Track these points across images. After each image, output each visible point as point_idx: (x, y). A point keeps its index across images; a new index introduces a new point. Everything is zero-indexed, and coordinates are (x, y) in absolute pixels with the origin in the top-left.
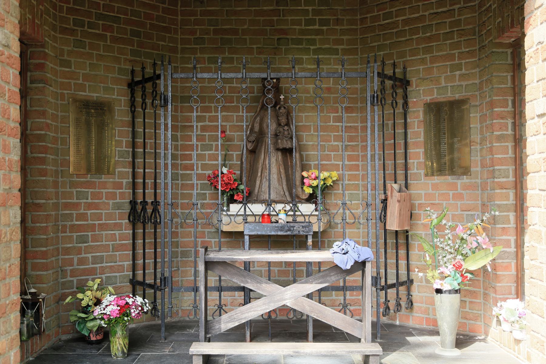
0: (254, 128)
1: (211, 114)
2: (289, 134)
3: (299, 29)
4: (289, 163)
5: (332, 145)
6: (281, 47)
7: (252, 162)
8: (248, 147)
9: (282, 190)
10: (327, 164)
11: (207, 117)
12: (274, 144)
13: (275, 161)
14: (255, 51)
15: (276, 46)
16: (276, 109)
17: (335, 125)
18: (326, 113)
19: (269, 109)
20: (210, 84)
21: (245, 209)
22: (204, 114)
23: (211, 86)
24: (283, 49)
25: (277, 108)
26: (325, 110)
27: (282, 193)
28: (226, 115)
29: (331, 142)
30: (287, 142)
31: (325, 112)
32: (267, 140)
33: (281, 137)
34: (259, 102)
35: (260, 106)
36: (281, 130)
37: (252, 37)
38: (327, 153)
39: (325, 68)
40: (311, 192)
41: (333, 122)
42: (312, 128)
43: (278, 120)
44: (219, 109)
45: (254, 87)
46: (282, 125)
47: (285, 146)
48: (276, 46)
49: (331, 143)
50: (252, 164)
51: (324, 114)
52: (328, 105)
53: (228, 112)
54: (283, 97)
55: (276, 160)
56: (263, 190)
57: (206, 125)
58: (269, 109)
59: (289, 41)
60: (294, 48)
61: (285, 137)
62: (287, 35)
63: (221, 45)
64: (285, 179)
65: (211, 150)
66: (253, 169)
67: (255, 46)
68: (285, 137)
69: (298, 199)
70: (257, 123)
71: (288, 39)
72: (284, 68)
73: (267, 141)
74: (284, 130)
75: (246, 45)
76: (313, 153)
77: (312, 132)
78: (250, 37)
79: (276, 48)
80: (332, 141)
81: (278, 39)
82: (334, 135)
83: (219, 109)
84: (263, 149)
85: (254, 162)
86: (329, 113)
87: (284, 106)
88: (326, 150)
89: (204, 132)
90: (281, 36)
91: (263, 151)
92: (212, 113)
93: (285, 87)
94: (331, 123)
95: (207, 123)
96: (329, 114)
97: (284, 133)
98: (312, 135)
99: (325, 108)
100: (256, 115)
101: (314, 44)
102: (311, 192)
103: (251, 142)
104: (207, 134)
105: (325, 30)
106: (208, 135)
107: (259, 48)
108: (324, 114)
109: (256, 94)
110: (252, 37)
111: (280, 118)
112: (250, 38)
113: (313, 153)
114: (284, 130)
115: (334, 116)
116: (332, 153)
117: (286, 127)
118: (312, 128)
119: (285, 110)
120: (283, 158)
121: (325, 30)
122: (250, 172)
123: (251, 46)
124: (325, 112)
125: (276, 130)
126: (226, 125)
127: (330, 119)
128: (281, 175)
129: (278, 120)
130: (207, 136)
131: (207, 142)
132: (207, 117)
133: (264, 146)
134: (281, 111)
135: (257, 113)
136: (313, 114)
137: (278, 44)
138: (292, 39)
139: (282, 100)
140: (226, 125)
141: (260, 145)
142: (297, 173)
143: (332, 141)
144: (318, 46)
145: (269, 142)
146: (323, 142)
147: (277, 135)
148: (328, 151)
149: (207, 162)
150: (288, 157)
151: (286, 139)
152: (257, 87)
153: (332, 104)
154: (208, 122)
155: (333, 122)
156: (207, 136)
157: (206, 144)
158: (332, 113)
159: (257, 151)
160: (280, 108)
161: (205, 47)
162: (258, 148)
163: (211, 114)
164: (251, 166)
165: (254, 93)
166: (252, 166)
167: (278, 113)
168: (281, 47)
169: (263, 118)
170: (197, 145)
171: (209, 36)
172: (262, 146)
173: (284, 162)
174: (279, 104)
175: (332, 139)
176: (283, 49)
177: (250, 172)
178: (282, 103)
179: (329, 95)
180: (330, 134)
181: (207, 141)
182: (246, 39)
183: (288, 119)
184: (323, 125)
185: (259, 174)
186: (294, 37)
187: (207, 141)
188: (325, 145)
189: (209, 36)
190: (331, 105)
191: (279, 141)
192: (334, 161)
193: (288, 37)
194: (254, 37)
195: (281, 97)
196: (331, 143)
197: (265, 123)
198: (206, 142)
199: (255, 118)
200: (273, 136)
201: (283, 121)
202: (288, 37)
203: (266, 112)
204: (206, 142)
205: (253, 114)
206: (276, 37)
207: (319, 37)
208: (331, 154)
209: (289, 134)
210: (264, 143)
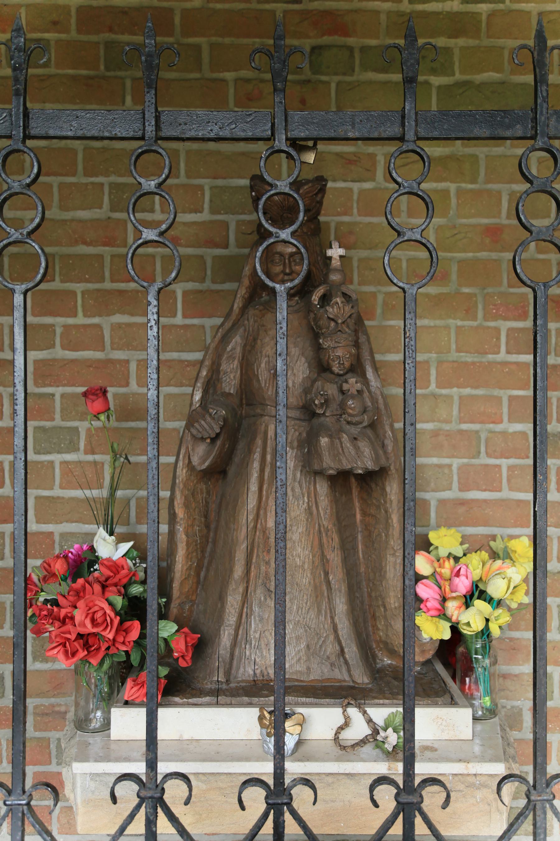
0: (219, 380)
1: (70, 321)
2: (365, 411)
3: (389, 13)
4: (358, 517)
5: (504, 433)
6: (324, 78)
7: (213, 507)
8: (195, 460)
9: (332, 637)
10: (485, 501)
11: (59, 331)
12: (300, 446)
13: (303, 517)
14: (232, 91)
15: (308, 74)
16: (309, 304)
17: (517, 364)
18: (485, 319)
19: (282, 304)
20: (67, 209)
21: (151, 823)
22: (48, 320)
23: (72, 220)
24: (333, 86)
25: (315, 298)
26: (480, 306)
27: (331, 648)
28: (129, 325)
29: (501, 422)
30: (357, 448)
31: (480, 314)
32: (271, 428)
33: (328, 421)
34: (238, 279)
35: (243, 292)
36: (332, 390)
37: (220, 40)
38: (484, 460)
39: (482, 156)
40: (447, 635)
41: (508, 352)
42: (433, 372)
43: (318, 348)
44: (18, 299)
45: (225, 225)
46: (336, 369)
47: (346, 466)
48: (308, 74)
49: (499, 428)
50: (212, 516)
51: (475, 324)
52: (490, 290)
53: (132, 315)
54: (341, 252)
55: (309, 511)
56: (254, 635)
57: (54, 360)
58: (282, 304)
59: (352, 55)
60: (371, 82)
61: (349, 423)
62: (346, 34)
63: (107, 68)
64: (344, 588)
65: (73, 448)
66: (215, 542)
67: (229, 76)
68: (349, 423)
69: (389, 658)
70: (231, 358)
71: (351, 49)
72: (337, 154)
73: (271, 433)
74: (342, 392)
75: (200, 70)
76: (435, 460)
77: (433, 386)
78: (214, 39)
79: (309, 81)
80: (505, 418)
81: (314, 49)
82: (511, 399)
83: (18, 299)
84: (256, 465)
85: (219, 513)
86: (496, 318)
87: (344, 289)
88: (483, 449)
89: (45, 386)
90: (326, 40)
91: (255, 475)
92: (75, 315)
93: (339, 225)
94: (503, 356)
95: (59, 353)
96: (492, 324)
97: (343, 406)
98: (435, 396)
99: (480, 299)
100: (228, 325)
101: (447, 70)
102: (447, 635)
103: (203, 439)
104: (58, 391)
105: (484, 18)
106: (63, 396)
107: (247, 81)
108: (475, 324)
109: (233, 250)
110: (220, 40)
111: (326, 343)
112: (212, 46)
113: (435, 460)
114: (342, 392)
115: (510, 331)
116: (504, 463)
117: (352, 380)
118: (433, 372)
119: (347, 308)
120: (335, 501)
121: (484, 18)
122: (203, 551)
123: (215, 75)
124: (480, 314)
125: (306, 391)
126: (127, 362)
127: (498, 339)
128: (327, 574)
129: (318, 348)
130: (58, 398)
131: (58, 421)
132: (59, 331)
133: (257, 456)
134: (332, 311)
135: (234, 317)
136: (438, 322)
137: (315, 69)
138: (364, 49)
139: (336, 263)
140: (127, 362)
141: (241, 445)
142: (390, 559)
143: (505, 418)
144: (458, 76)
145: (282, 439)
146: (472, 422)
147: (314, 415)
148: (488, 455)
149: (57, 492)
150: (355, 492)
151: (354, 430)
152: (239, 223)
153: (504, 288)
154: (63, 348)
155: (508, 352)
156: (58, 398)
157: (54, 428)
158: (506, 319)
159: (232, 471)
160: (325, 299)
161: (50, 76)
162: (237, 459)
163: (70, 321)
164: (208, 526)
165: (226, 247)
166: (213, 526)
167: (316, 320)
168: (324, 78)
169: (255, 340)
170: (142, 382)
171: (63, 36)
172: (250, 451)
173: (338, 518)
174: (325, 280)
175: (505, 410)
176: (333, 86)
177: (203, 551)
178: (335, 277)
179: (494, 255)
180: (496, 392)
181: (58, 416)
182: (198, 48)
183: (357, 345)
184: (473, 363)
185: (238, 571)
186: (373, 42)
187: (58, 416)
188: (477, 432)
189: (63, 36)
190: (503, 289)
191: (324, 441)
192: (511, 489)
193: (351, 41)
194: (227, 40)
195: (329, 253)
196: (499, 428)
197: (265, 360)
198: (53, 419)
199: (225, 339)
200: (293, 414)
201: (339, 353)
202: (351, 41)
203: (269, 316)
204: (53, 419)
205: (218, 321)
206: (307, 44)
207: (461, 42)
208: (499, 467)
209: (365, 411)
210: (259, 442)
